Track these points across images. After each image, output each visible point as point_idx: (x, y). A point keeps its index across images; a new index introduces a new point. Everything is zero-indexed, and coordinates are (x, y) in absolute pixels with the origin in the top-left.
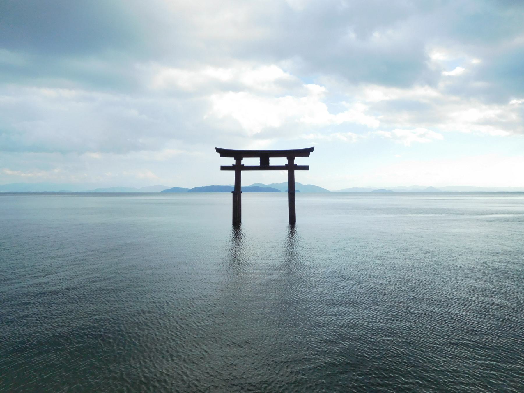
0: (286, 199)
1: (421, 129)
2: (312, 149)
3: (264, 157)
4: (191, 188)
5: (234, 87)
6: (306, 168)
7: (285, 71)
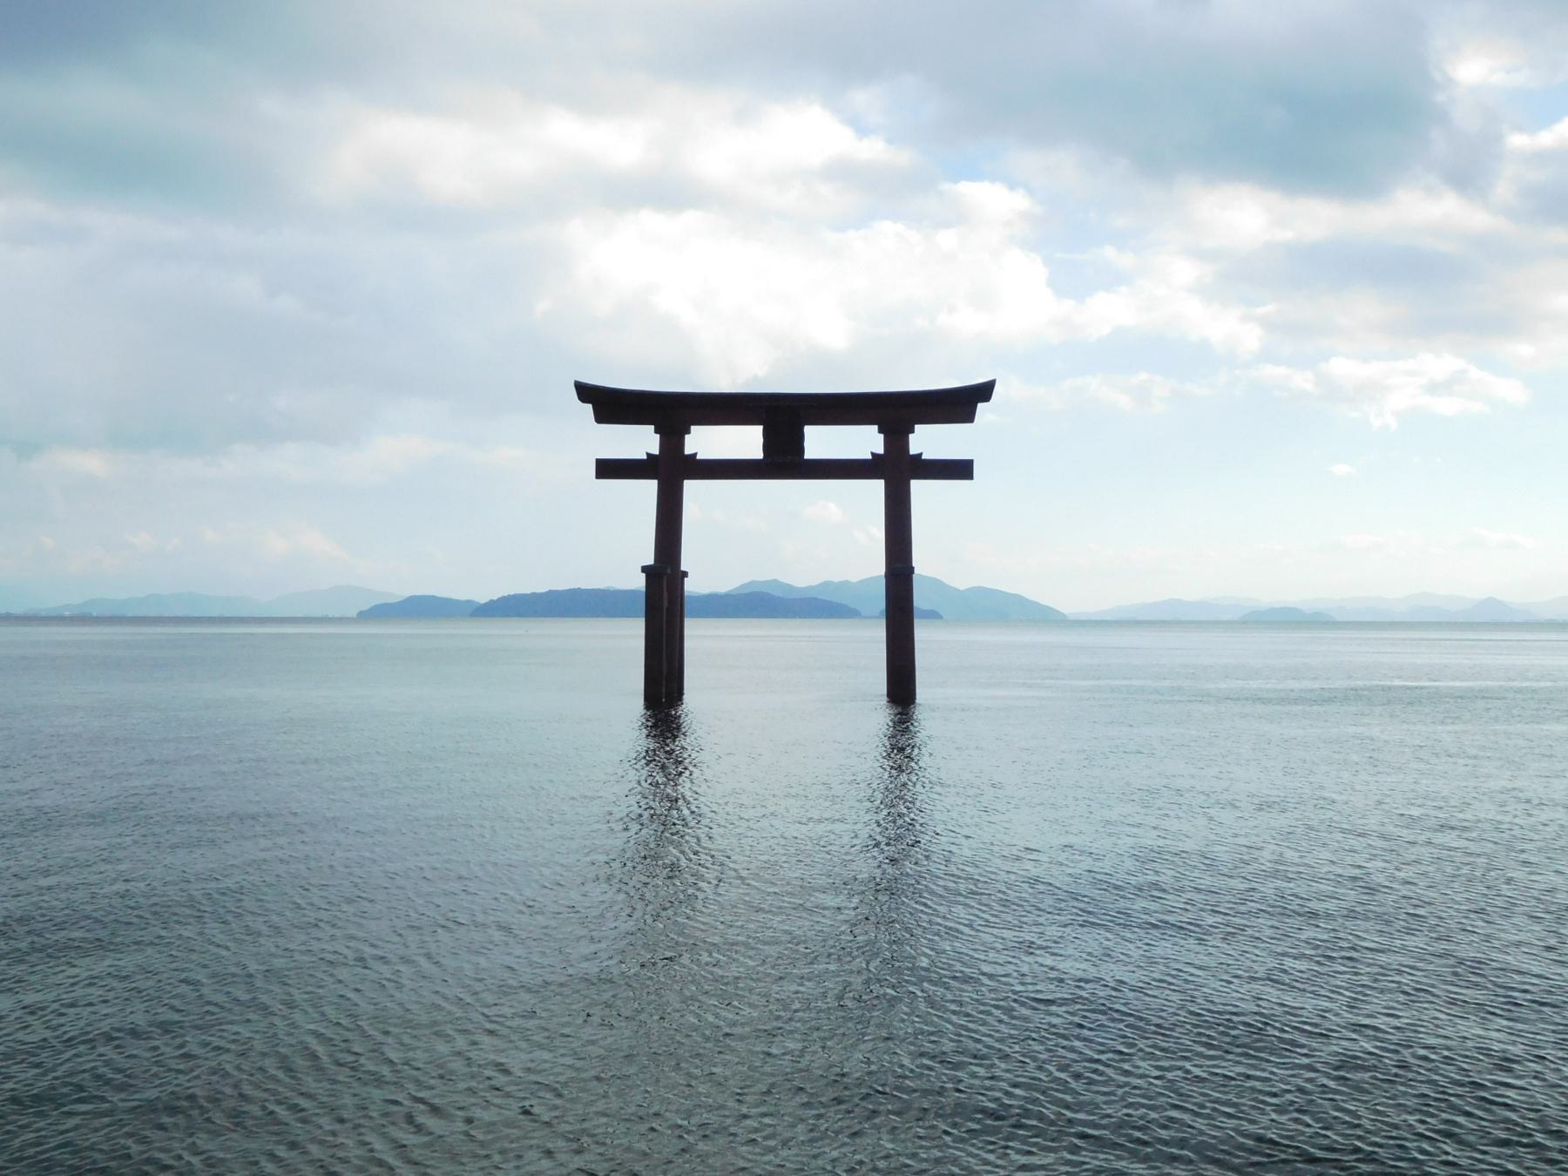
0: (877, 634)
1: (1439, 363)
2: (983, 392)
3: (783, 419)
4: (483, 597)
5: (663, 191)
6: (960, 470)
7: (862, 129)
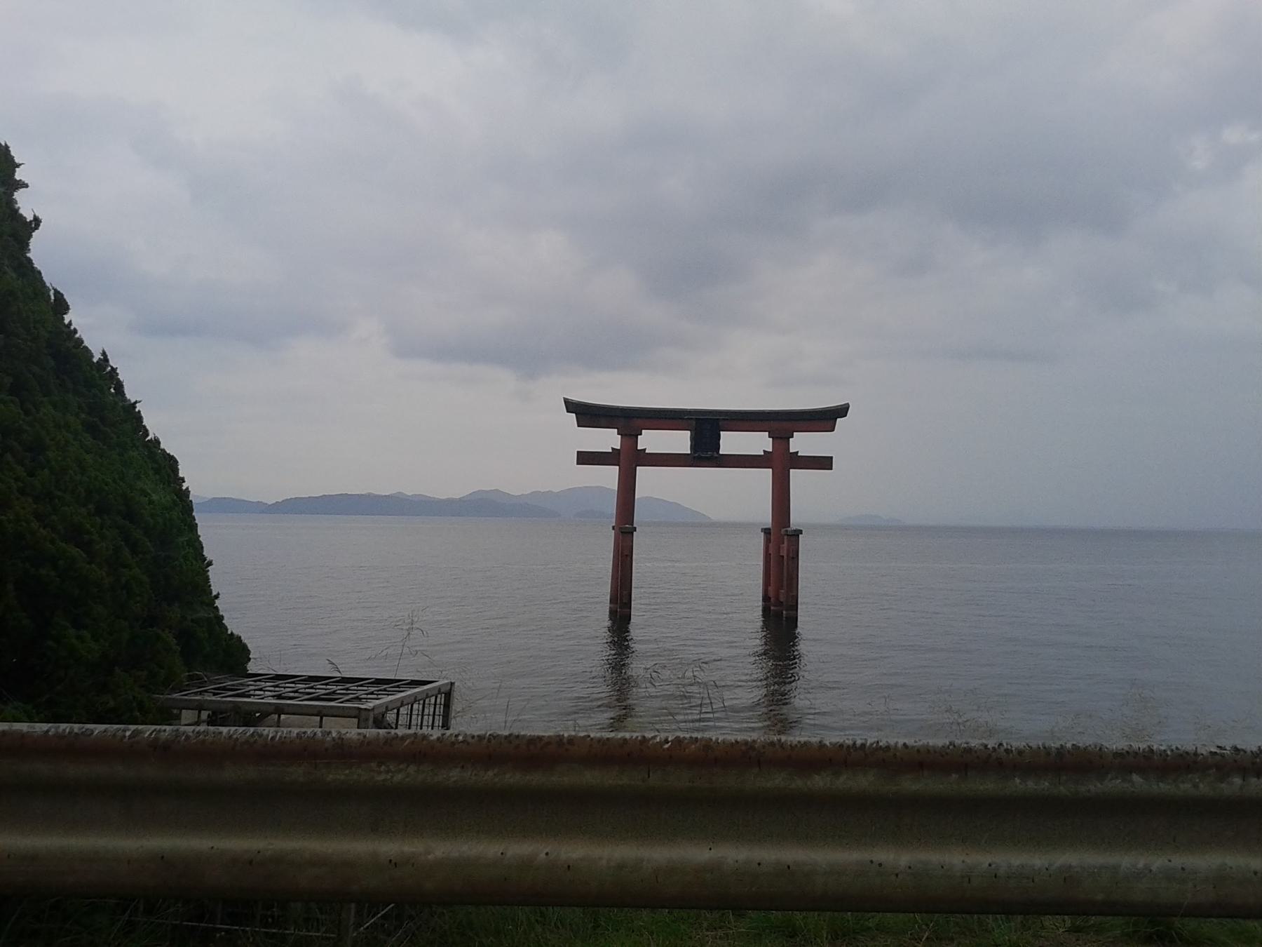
2: (842, 411)
3: (706, 429)
6: (824, 463)
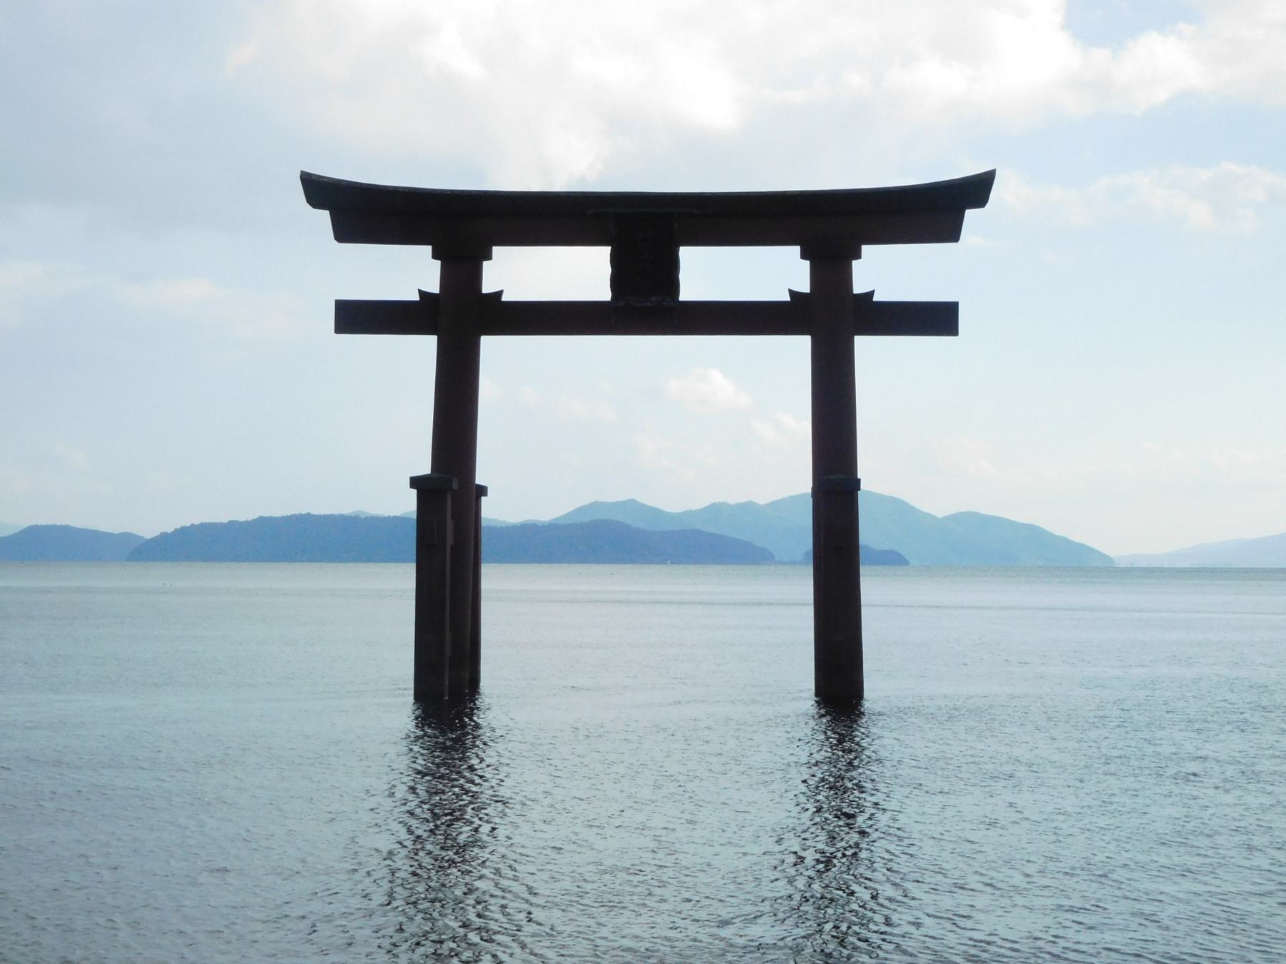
0: (800, 589)
2: (976, 190)
3: (646, 235)
4: (149, 526)
6: (936, 319)
